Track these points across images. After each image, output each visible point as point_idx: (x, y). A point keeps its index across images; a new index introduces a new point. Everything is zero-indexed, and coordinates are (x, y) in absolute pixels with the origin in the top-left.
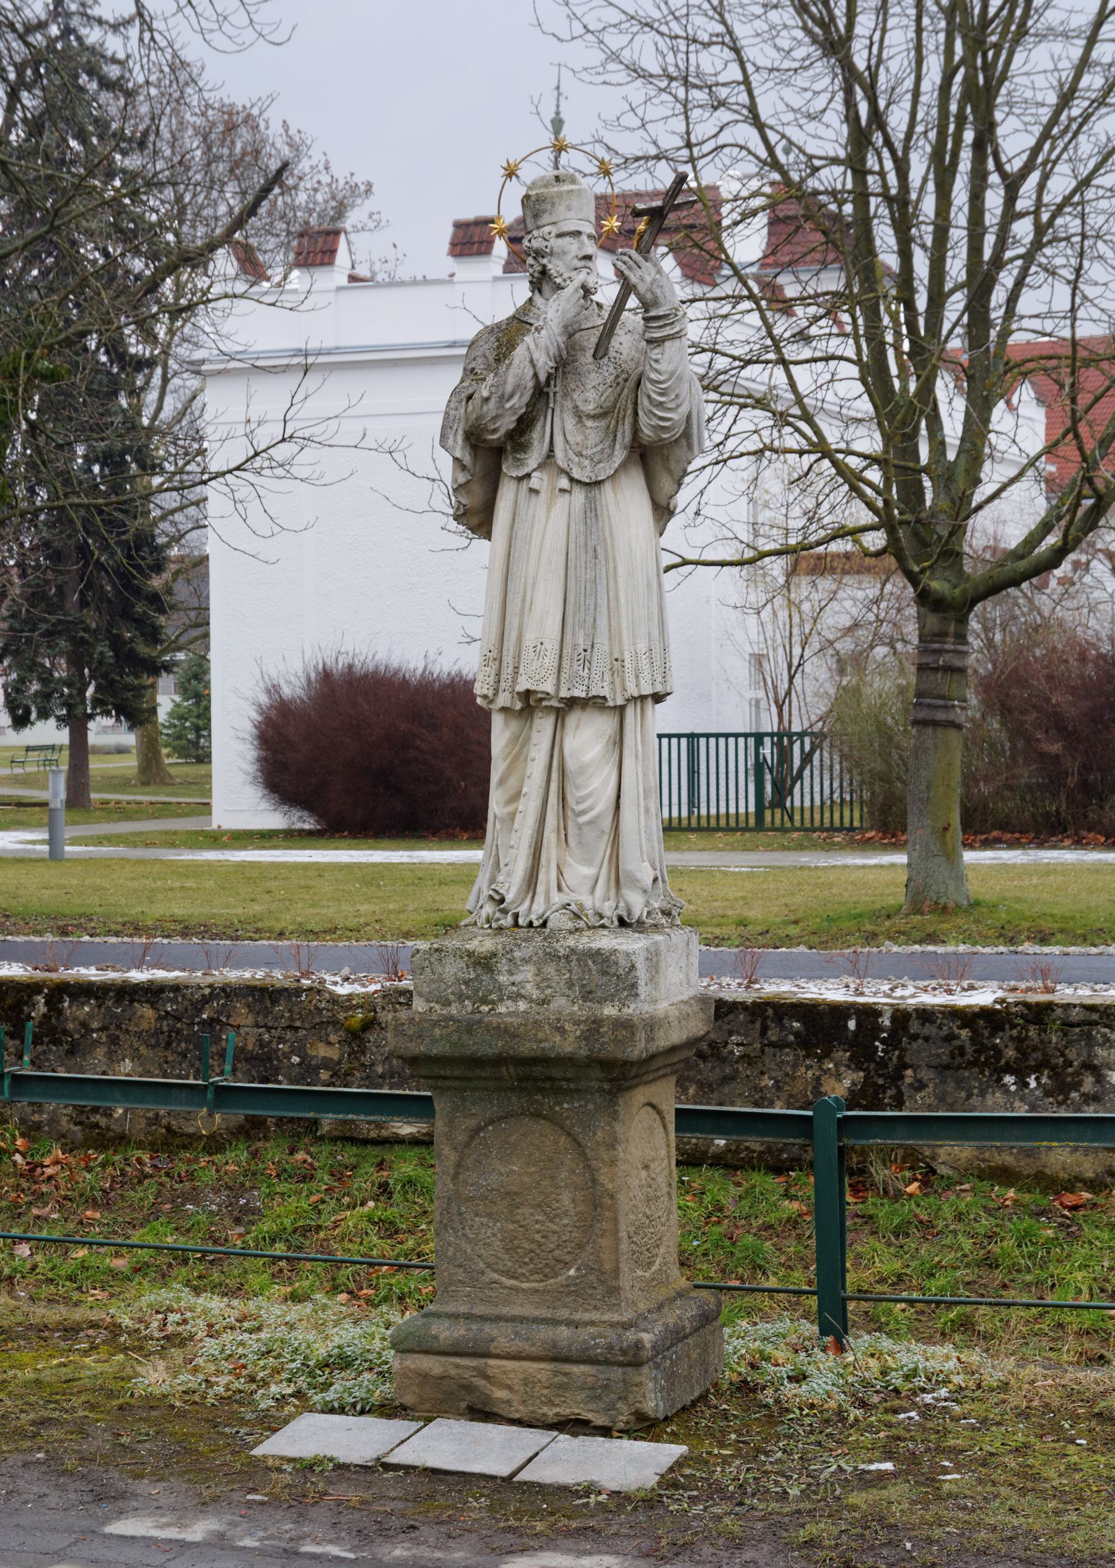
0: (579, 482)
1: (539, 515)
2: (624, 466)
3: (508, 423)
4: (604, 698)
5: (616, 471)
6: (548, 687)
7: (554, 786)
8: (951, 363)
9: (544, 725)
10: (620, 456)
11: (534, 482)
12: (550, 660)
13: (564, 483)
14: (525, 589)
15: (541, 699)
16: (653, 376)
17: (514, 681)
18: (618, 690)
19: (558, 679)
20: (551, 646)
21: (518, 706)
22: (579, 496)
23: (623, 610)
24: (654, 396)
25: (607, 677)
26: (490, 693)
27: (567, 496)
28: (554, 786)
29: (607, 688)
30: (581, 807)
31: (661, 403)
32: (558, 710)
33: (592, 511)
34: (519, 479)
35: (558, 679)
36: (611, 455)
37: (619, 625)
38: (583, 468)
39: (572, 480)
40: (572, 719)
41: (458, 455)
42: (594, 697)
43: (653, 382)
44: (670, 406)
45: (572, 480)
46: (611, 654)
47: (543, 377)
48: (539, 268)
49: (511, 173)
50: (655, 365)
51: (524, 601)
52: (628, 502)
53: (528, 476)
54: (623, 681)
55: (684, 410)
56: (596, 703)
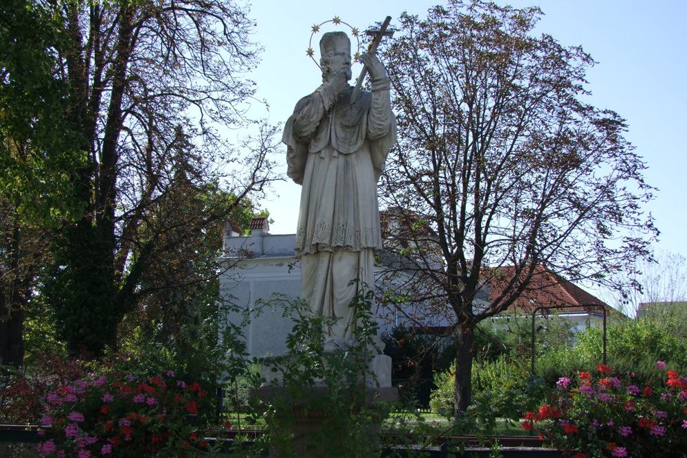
0: (342, 154)
1: (325, 168)
2: (361, 148)
3: (312, 128)
4: (351, 247)
5: (358, 150)
6: (326, 241)
7: (328, 287)
8: (460, 270)
9: (325, 259)
10: (360, 143)
11: (322, 155)
12: (328, 231)
13: (335, 154)
14: (317, 199)
15: (323, 247)
16: (375, 106)
17: (312, 240)
18: (358, 244)
19: (331, 239)
20: (328, 223)
21: (313, 252)
22: (341, 160)
23: (360, 209)
24: (375, 114)
25: (353, 237)
26: (301, 247)
27: (336, 159)
28: (328, 287)
29: (352, 243)
30: (341, 296)
31: (379, 118)
32: (331, 253)
33: (347, 164)
34: (316, 153)
35: (331, 239)
36: (356, 143)
37: (358, 215)
38: (344, 148)
39: (339, 152)
40: (337, 256)
41: (290, 144)
42: (348, 246)
43: (375, 108)
44: (382, 119)
45: (339, 152)
46: (355, 228)
47: (327, 108)
48: (327, 69)
49: (316, 29)
50: (377, 101)
51: (317, 204)
52: (363, 167)
53: (320, 152)
54: (360, 241)
55: (388, 121)
56: (347, 248)
